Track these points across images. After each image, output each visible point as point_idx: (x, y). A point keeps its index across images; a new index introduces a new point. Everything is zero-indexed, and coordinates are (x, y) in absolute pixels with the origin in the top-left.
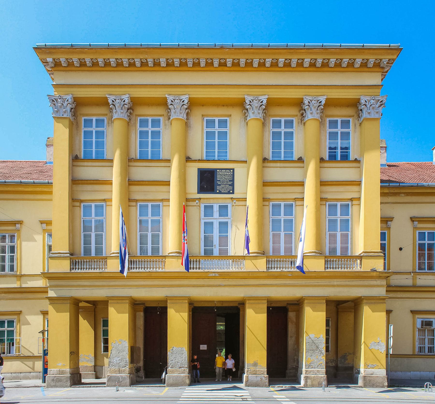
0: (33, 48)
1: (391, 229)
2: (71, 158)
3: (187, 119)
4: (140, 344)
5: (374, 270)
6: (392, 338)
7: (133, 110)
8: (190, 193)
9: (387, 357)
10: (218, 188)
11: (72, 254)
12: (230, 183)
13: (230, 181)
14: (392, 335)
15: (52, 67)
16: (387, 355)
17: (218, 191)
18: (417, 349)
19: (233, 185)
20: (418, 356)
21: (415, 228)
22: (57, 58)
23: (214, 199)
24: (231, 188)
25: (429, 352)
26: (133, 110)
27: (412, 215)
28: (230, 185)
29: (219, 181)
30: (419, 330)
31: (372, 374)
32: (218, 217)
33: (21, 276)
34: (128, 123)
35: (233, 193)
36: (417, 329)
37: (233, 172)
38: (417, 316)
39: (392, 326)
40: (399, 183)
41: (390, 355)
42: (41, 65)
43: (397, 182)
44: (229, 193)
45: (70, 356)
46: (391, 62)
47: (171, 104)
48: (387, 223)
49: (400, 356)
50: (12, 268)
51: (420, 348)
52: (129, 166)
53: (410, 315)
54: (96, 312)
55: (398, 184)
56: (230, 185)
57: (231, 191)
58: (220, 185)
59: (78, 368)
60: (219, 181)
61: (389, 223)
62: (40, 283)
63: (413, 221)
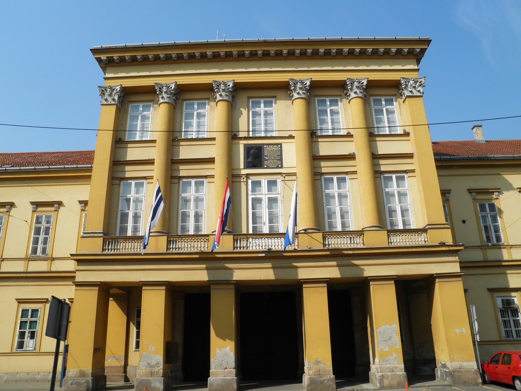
0: (91, 50)
1: (451, 201)
2: (114, 140)
3: (233, 101)
4: (179, 339)
5: (443, 244)
6: (476, 322)
7: (180, 96)
8: (236, 169)
9: (474, 345)
10: (266, 163)
11: (104, 234)
12: (279, 158)
13: (278, 156)
14: (475, 318)
15: (105, 64)
16: (474, 342)
17: (266, 166)
18: (503, 334)
19: (281, 160)
20: (506, 342)
21: (474, 199)
22: (111, 59)
23: (262, 175)
24: (279, 162)
25: (517, 337)
26: (180, 96)
27: (469, 187)
28: (278, 160)
29: (267, 156)
30: (501, 310)
31: (460, 368)
32: (267, 192)
33: (53, 259)
34: (174, 106)
35: (282, 167)
36: (499, 310)
37: (281, 147)
38: (496, 294)
39: (474, 307)
40: (451, 155)
41: (478, 342)
42: (96, 63)
43: (449, 155)
44: (277, 167)
45: (94, 354)
46: (423, 51)
47: (217, 88)
48: (445, 196)
49: (492, 343)
50: (44, 251)
51: (507, 332)
52: (173, 145)
53: (488, 295)
54: (129, 298)
55: (449, 157)
56: (278, 160)
57: (280, 166)
58: (267, 160)
59: (103, 368)
60: (267, 156)
61: (447, 195)
62: (70, 266)
63: (471, 193)
